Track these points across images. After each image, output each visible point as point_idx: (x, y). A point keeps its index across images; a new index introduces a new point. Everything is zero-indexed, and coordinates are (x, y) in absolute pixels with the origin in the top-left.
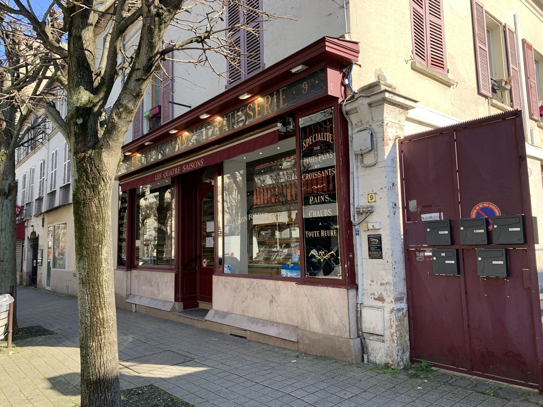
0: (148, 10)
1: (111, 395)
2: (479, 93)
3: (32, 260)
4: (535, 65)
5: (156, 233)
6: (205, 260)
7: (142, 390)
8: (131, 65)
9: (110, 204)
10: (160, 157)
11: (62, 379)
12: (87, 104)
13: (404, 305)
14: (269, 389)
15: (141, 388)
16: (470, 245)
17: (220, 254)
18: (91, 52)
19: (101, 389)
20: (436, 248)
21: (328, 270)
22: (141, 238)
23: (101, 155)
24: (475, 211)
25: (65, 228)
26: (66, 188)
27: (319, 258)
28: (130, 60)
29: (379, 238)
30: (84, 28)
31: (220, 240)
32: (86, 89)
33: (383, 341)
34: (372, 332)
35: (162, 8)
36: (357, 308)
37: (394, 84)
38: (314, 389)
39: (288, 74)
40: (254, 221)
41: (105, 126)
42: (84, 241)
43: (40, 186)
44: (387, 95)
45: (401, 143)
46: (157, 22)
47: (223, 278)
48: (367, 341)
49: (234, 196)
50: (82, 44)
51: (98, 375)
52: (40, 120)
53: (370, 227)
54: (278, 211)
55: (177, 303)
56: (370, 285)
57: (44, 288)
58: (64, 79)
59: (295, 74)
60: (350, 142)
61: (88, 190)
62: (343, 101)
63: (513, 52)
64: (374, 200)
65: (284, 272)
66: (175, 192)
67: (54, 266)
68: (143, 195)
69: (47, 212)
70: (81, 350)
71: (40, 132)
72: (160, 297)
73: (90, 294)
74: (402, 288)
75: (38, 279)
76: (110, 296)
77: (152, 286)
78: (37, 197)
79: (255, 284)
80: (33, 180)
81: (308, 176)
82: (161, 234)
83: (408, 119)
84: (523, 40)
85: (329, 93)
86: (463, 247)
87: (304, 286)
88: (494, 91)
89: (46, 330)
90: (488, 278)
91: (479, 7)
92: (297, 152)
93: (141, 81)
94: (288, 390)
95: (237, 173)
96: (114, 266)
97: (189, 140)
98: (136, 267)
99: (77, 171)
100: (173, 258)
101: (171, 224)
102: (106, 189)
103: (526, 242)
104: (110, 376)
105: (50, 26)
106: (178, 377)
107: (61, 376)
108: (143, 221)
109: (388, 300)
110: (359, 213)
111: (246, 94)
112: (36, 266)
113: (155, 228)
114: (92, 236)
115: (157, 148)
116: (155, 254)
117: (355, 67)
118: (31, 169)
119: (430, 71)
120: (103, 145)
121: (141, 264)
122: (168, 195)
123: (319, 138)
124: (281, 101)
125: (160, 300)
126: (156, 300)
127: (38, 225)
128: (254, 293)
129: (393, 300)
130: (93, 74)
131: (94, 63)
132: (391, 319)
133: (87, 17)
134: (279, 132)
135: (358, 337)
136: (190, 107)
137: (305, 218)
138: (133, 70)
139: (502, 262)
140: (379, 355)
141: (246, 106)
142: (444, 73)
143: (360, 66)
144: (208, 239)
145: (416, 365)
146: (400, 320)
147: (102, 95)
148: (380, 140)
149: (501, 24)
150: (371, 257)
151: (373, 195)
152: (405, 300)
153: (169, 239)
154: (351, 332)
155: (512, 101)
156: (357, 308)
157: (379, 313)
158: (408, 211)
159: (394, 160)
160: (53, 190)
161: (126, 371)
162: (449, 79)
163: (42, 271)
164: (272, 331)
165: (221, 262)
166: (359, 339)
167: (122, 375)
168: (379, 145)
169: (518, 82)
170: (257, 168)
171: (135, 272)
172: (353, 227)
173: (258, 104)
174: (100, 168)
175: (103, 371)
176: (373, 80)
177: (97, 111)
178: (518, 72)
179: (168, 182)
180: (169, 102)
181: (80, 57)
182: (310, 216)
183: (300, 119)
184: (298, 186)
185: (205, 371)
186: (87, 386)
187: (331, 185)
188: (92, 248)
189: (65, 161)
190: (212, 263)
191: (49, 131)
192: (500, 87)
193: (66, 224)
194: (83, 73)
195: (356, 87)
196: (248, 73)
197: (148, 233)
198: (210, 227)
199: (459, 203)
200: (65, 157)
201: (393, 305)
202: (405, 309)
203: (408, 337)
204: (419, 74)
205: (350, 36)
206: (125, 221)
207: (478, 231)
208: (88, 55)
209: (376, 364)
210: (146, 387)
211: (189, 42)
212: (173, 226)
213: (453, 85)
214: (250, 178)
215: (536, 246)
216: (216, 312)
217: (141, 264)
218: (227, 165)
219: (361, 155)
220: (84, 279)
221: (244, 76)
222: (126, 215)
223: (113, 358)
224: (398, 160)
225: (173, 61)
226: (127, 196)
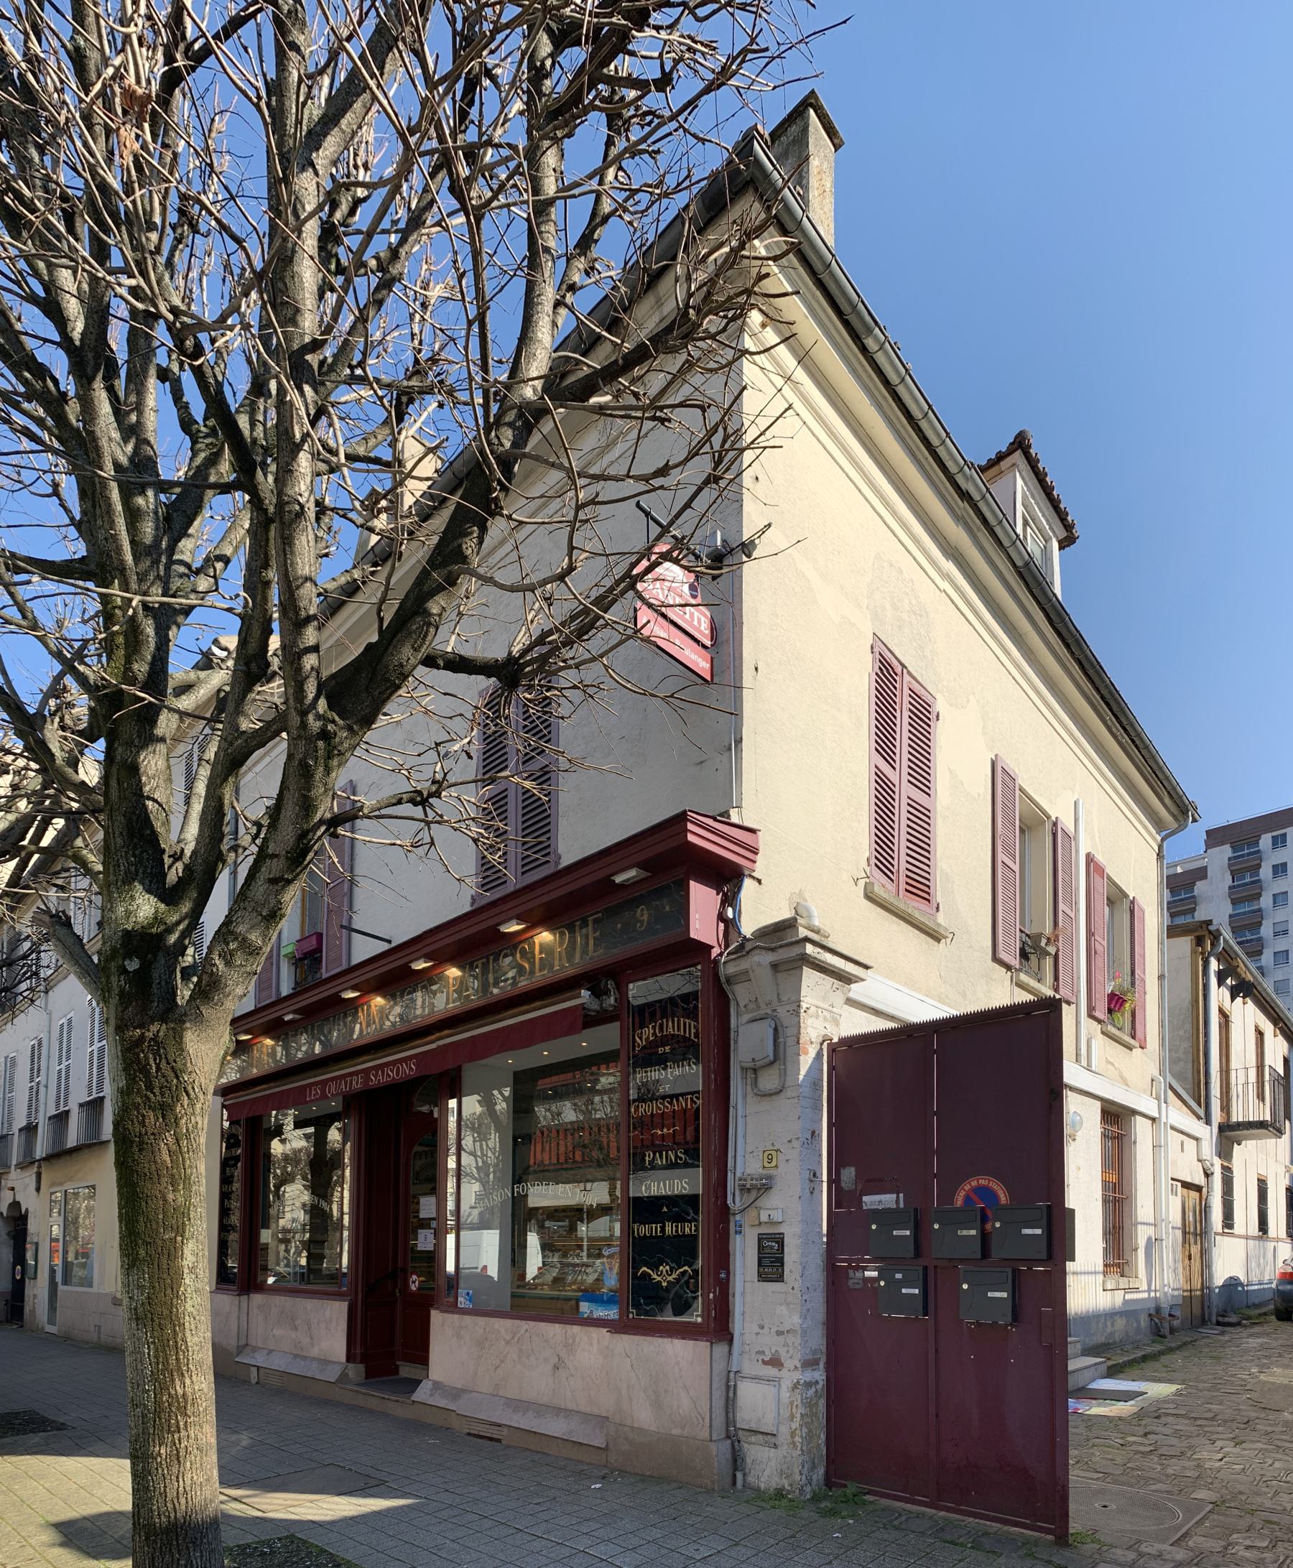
0: (302, 722)
1: (202, 1556)
2: (996, 959)
3: (10, 1266)
4: (1107, 909)
5: (308, 1217)
6: (414, 1277)
7: (270, 1547)
8: (258, 841)
9: (203, 1147)
10: (318, 1049)
11: (89, 1525)
12: (151, 925)
13: (819, 1375)
14: (544, 1542)
15: (268, 1543)
16: (950, 1260)
17: (450, 1267)
18: (160, 805)
19: (178, 1545)
20: (888, 1263)
21: (682, 1307)
22: (273, 1225)
23: (181, 1038)
24: (963, 1194)
25: (92, 1197)
26: (94, 1106)
27: (659, 1279)
28: (254, 830)
29: (780, 1239)
30: (144, 746)
31: (451, 1239)
32: (149, 891)
33: (775, 1446)
34: (754, 1427)
35: (333, 722)
36: (728, 1380)
37: (826, 928)
38: (635, 1541)
39: (607, 886)
40: (530, 1199)
41: (195, 979)
42: (141, 1227)
43: (30, 1100)
44: (810, 949)
45: (833, 1049)
46: (321, 753)
47: (456, 1316)
48: (745, 1445)
49: (491, 1144)
50: (140, 786)
51: (172, 1515)
52: (27, 945)
53: (764, 1218)
54: (588, 1181)
55: (350, 1365)
56: (757, 1334)
57: (43, 1328)
58: (91, 858)
59: (622, 886)
60: (732, 1042)
61: (151, 1114)
62: (721, 954)
63: (1067, 879)
64: (774, 1164)
65: (585, 1307)
66: (352, 1130)
67: (66, 1281)
68: (278, 1131)
69: (48, 1158)
70: (133, 1465)
71: (25, 973)
72: (315, 1352)
73: (154, 1343)
74: (818, 1340)
75: (27, 1309)
76: (201, 1347)
77: (296, 1328)
78: (23, 1123)
79: (523, 1331)
80: (12, 1084)
81: (644, 1109)
82: (319, 1219)
83: (850, 1002)
84: (1088, 855)
85: (692, 935)
86: (936, 1263)
87: (625, 1337)
88: (1024, 955)
89: (48, 1420)
90: (978, 1324)
91: (1007, 779)
92: (623, 1055)
93: (280, 882)
94: (582, 1544)
95: (495, 1092)
96: (210, 1282)
97: (384, 1014)
98: (261, 1288)
99: (124, 1070)
100: (345, 1270)
101: (342, 1197)
102: (194, 1114)
103: (1050, 1256)
104: (199, 1517)
105: (56, 725)
106: (352, 1518)
107: (85, 1518)
108: (278, 1187)
109: (789, 1364)
110: (744, 1189)
111: (515, 921)
112: (23, 1280)
113: (304, 1205)
114: (161, 1216)
115: (313, 1029)
116: (303, 1262)
117: (748, 883)
118: (6, 1058)
119: (902, 906)
120: (185, 1014)
121: (271, 1280)
122: (334, 1135)
123: (671, 1028)
124: (591, 942)
125: (314, 1359)
126: (305, 1358)
127: (26, 1186)
128: (520, 1350)
129: (799, 1365)
130: (166, 857)
131: (168, 831)
132: (792, 1403)
133: (153, 721)
134: (584, 1009)
135: (728, 1437)
136: (389, 942)
137: (635, 1199)
138: (262, 856)
139: (1005, 1295)
140: (766, 1473)
141: (515, 947)
142: (929, 910)
143: (759, 881)
144: (422, 1233)
145: (836, 1492)
146: (809, 1404)
147: (186, 907)
148: (791, 1041)
149: (1049, 817)
150: (763, 1277)
151: (774, 1153)
152: (822, 1365)
153: (335, 1229)
154: (714, 1428)
155: (1056, 978)
156: (728, 1380)
157: (770, 1390)
158: (839, 1189)
159: (816, 1085)
160: (62, 1109)
161: (234, 1508)
162: (939, 925)
163: (37, 1292)
164: (555, 1427)
165: (453, 1283)
166: (729, 1442)
167: (227, 1516)
168: (790, 1052)
169: (1072, 941)
170: (543, 1084)
171: (257, 1298)
172: (732, 1218)
173: (541, 945)
174: (179, 1066)
175: (183, 1508)
176: (786, 914)
177: (175, 943)
178: (1073, 920)
179: (335, 1105)
180: (342, 926)
181: (133, 813)
182: (644, 1192)
183: (631, 986)
184: (623, 1128)
185: (408, 1506)
186: (147, 1539)
187: (690, 1130)
188: (159, 1242)
189: (92, 1044)
190: (431, 1285)
191: (44, 973)
192: (1037, 947)
193: (93, 1187)
194: (142, 852)
195: (748, 927)
196: (523, 873)
197: (288, 1216)
198: (427, 1207)
199: (935, 1176)
200: (92, 1036)
201: (797, 1376)
202: (821, 1383)
203: (823, 1437)
204: (879, 910)
205: (740, 814)
206: (236, 1186)
207: (965, 1233)
208: (155, 810)
209: (758, 1490)
210: (279, 1539)
211: (394, 801)
212: (346, 1201)
213: (945, 937)
214: (522, 1106)
215: (1070, 1266)
216: (437, 1385)
217: (271, 1280)
218: (470, 1073)
219: (754, 1071)
220: (140, 1310)
221: (514, 880)
222: (238, 1172)
223: (208, 1480)
224: (825, 1084)
225: (353, 839)
226: (240, 1131)
